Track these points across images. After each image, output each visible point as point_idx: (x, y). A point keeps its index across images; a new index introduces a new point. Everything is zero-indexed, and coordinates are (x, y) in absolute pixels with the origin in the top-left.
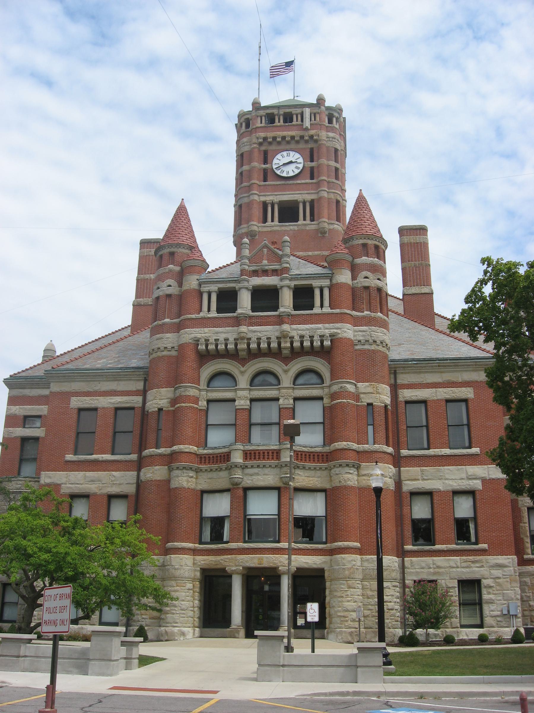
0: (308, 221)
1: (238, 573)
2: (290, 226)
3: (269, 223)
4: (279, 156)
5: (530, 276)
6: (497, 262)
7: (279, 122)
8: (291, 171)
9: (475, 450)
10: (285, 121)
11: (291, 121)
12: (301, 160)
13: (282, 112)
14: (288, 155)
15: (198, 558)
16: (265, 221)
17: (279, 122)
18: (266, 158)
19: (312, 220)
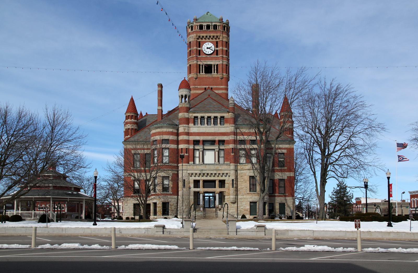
0: (216, 74)
1: (217, 193)
2: (208, 75)
3: (201, 73)
4: (205, 45)
5: (249, 110)
6: (20, 117)
7: (211, 29)
8: (209, 52)
9: (286, 168)
10: (200, 29)
11: (216, 29)
12: (213, 47)
13: (213, 24)
14: (208, 44)
15: (117, 206)
16: (200, 73)
17: (211, 29)
18: (199, 45)
19: (217, 73)
